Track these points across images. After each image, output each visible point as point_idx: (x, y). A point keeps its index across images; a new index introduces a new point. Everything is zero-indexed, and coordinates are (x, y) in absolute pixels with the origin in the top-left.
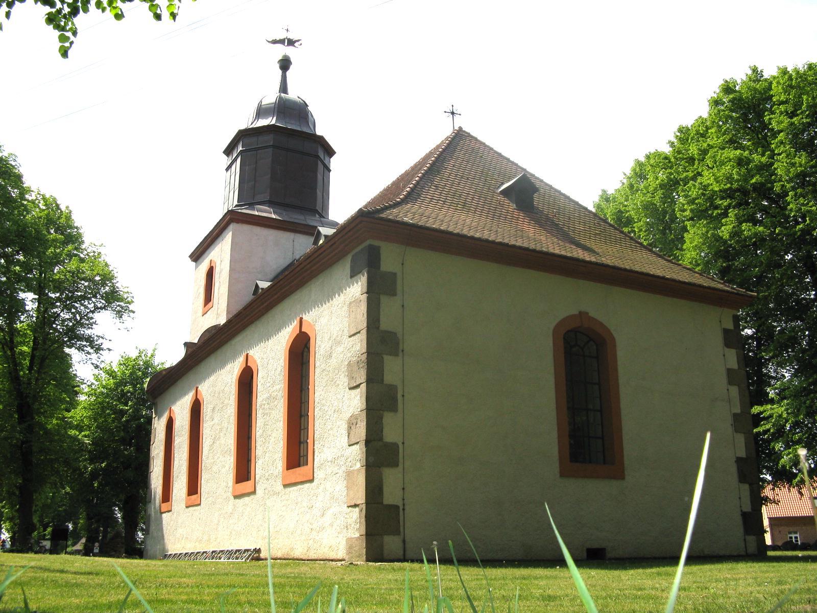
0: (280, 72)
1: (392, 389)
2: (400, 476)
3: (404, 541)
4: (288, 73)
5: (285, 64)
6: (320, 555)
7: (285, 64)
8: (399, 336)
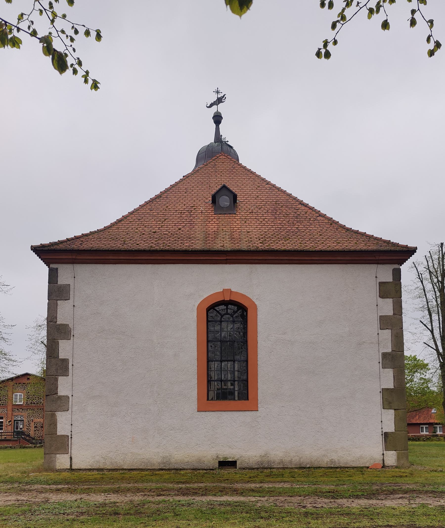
0: (215, 125)
1: (65, 361)
2: (70, 416)
3: (71, 458)
4: (220, 126)
5: (218, 119)
6: (101, 465)
7: (218, 119)
8: (71, 326)
